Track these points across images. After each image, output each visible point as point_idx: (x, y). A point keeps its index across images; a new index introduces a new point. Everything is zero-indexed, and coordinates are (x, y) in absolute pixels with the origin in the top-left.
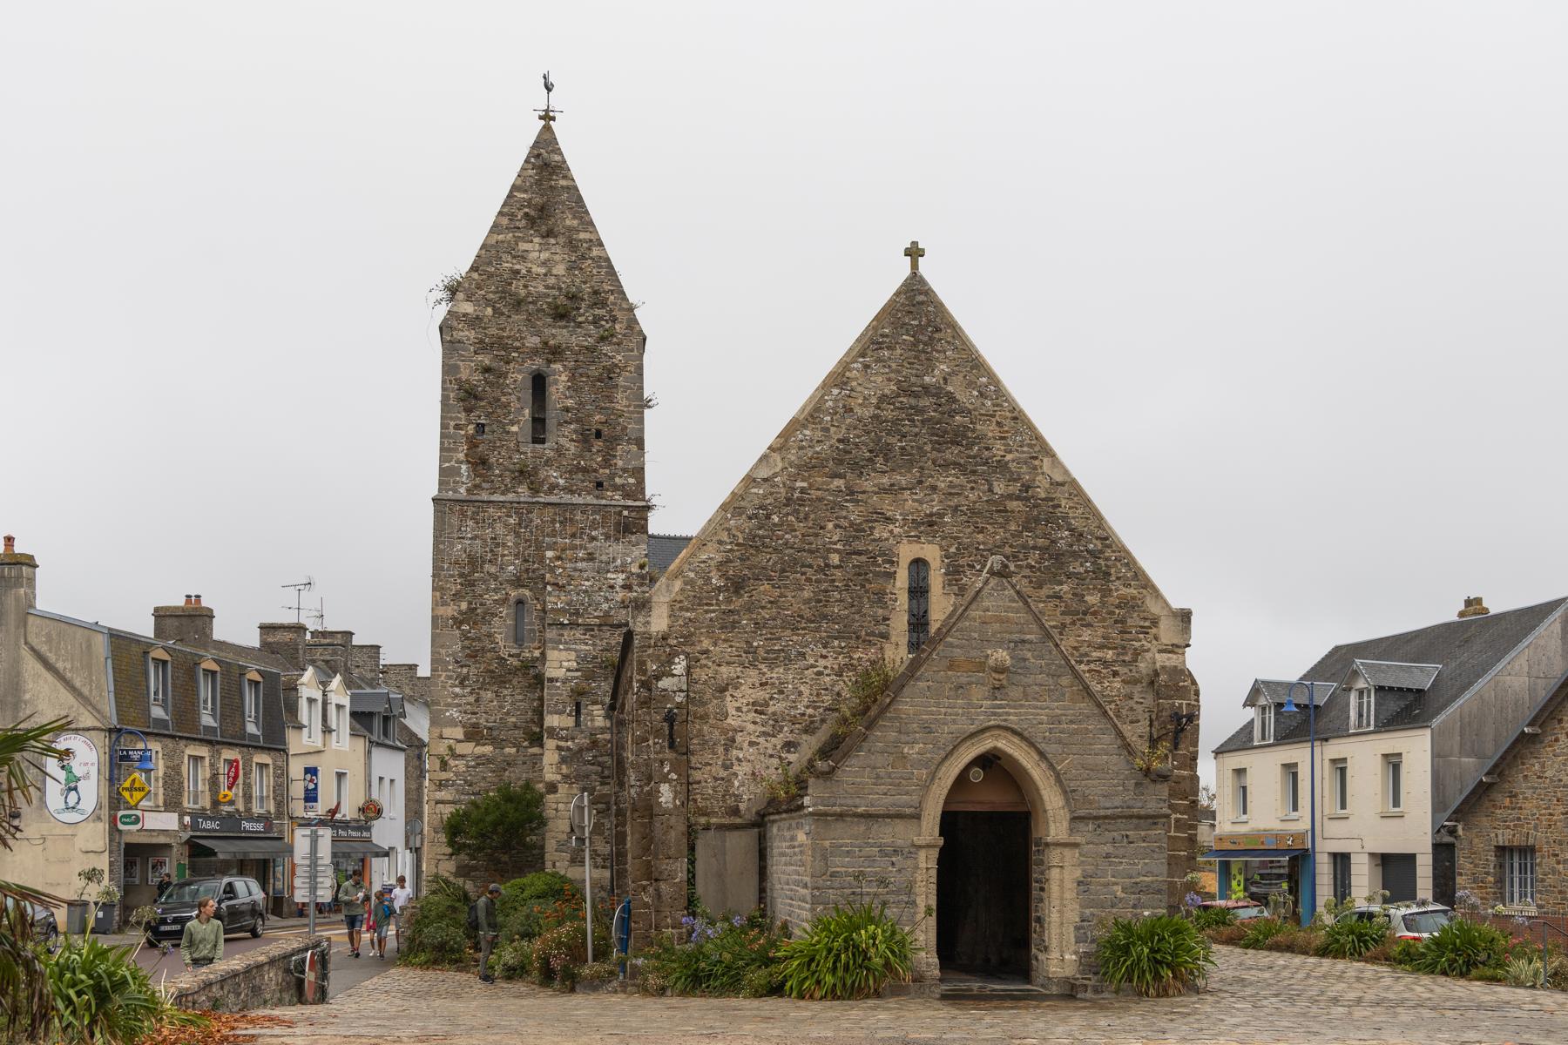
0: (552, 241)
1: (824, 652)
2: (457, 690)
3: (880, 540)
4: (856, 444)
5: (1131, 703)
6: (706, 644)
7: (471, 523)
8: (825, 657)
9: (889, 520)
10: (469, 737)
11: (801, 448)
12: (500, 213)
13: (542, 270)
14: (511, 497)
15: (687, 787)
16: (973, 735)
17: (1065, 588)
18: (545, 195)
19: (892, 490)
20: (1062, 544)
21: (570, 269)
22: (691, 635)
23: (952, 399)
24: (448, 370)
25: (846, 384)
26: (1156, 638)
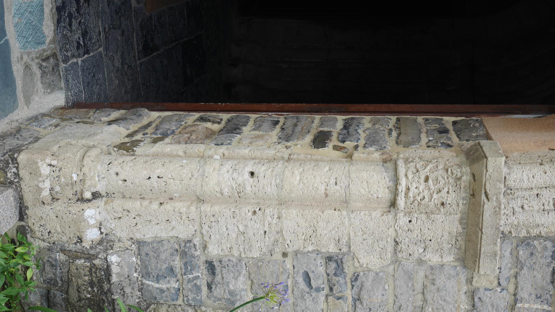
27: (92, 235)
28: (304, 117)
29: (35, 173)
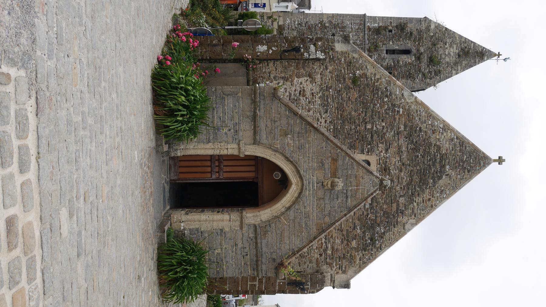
0: (457, 57)
1: (328, 122)
2: (297, 22)
3: (378, 147)
4: (419, 136)
5: (308, 263)
6: (330, 68)
7: (357, 27)
8: (326, 121)
9: (387, 150)
10: (279, 27)
11: (417, 111)
12: (466, 38)
13: (447, 53)
14: (367, 42)
15: (265, 59)
16: (298, 172)
17: (359, 231)
18: (472, 54)
19: (399, 152)
20: (378, 229)
21: (448, 63)
22: (334, 62)
23: (440, 178)
24: (411, 20)
25: (445, 130)
26: (337, 273)
27: (182, 228)
28: (215, 209)
29: (174, 218)
